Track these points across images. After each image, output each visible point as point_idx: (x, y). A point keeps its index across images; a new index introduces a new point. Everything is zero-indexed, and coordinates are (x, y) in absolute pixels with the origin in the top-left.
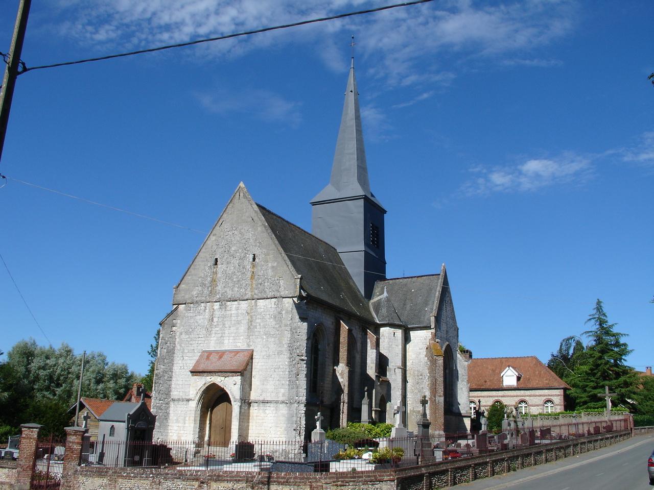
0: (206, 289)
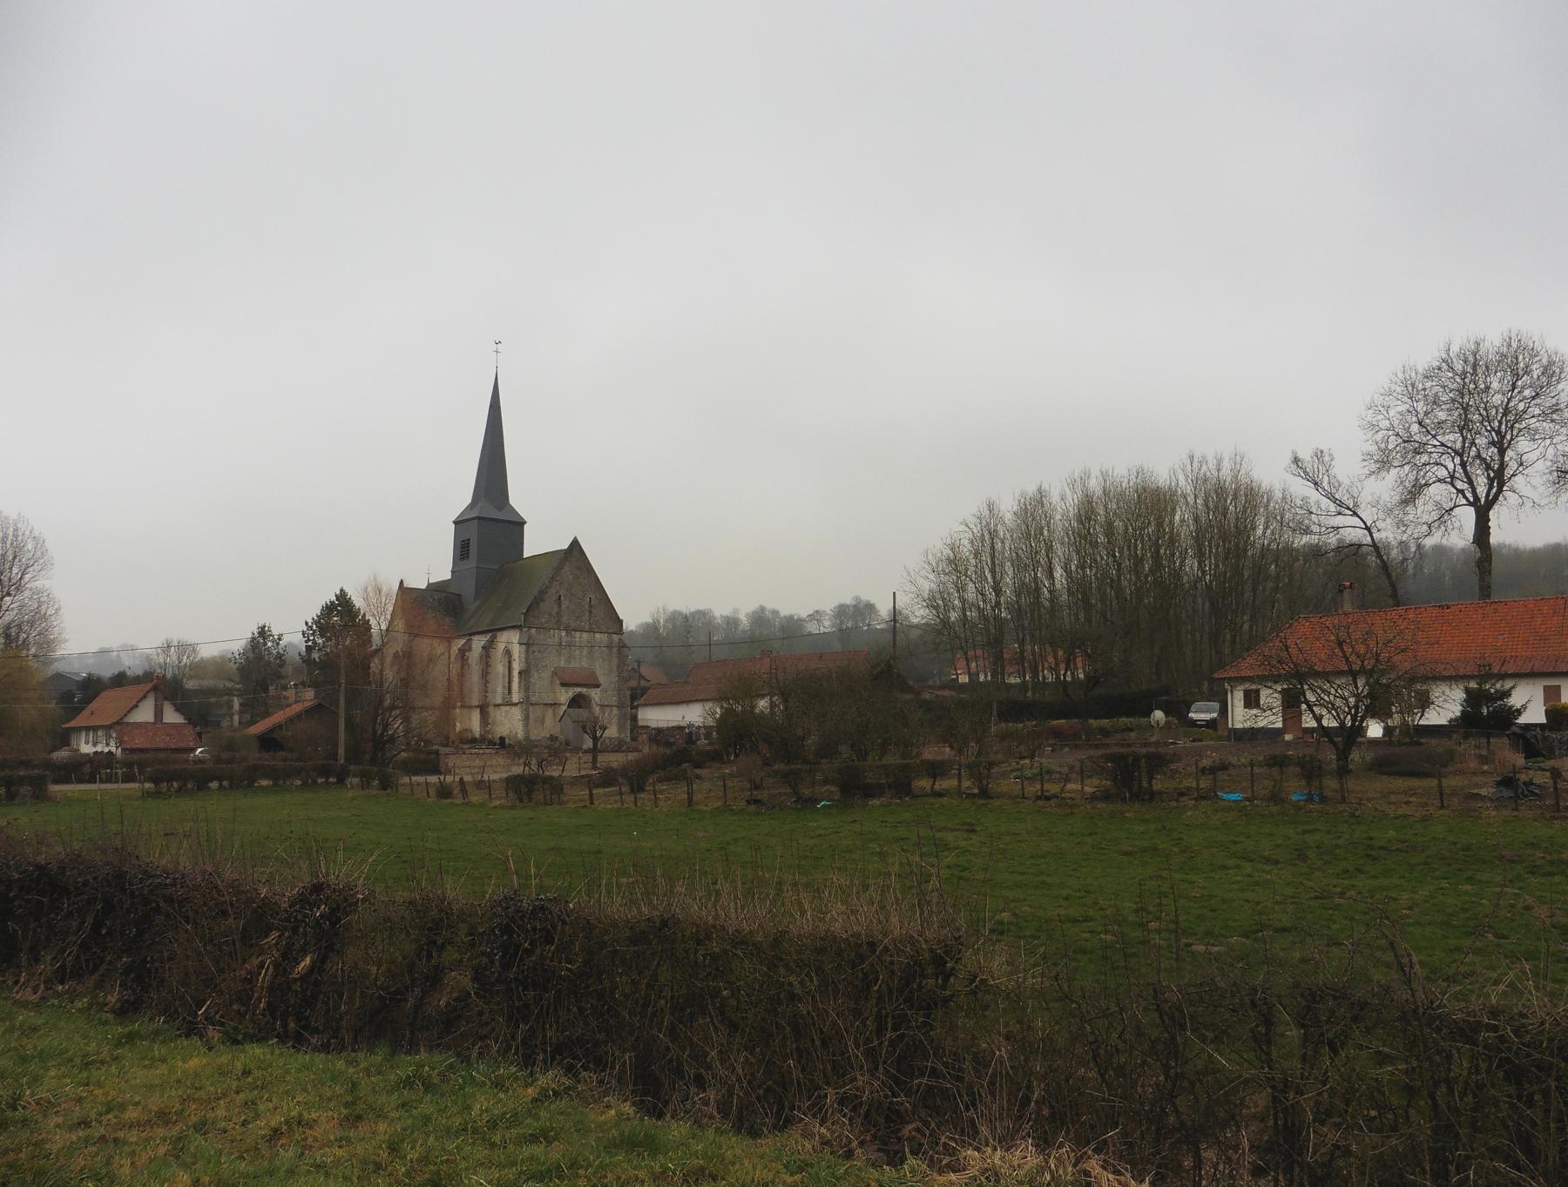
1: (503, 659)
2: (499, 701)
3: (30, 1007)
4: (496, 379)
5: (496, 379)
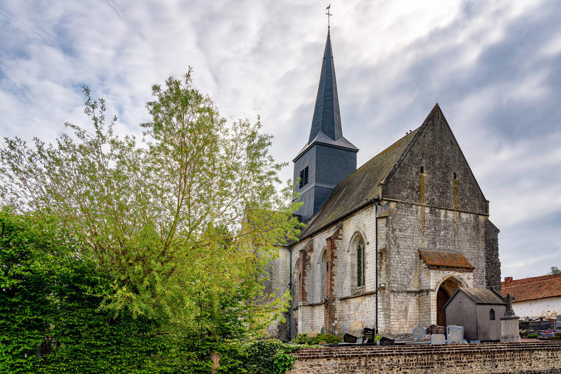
0: (415, 192)
1: (351, 248)
2: (347, 293)
3: (192, 118)
4: (329, 36)
5: (329, 36)
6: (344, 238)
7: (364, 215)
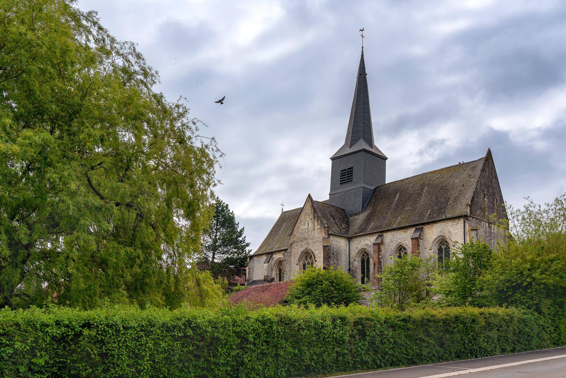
4: (362, 55)
5: (362, 55)
6: (425, 239)
7: (450, 224)
